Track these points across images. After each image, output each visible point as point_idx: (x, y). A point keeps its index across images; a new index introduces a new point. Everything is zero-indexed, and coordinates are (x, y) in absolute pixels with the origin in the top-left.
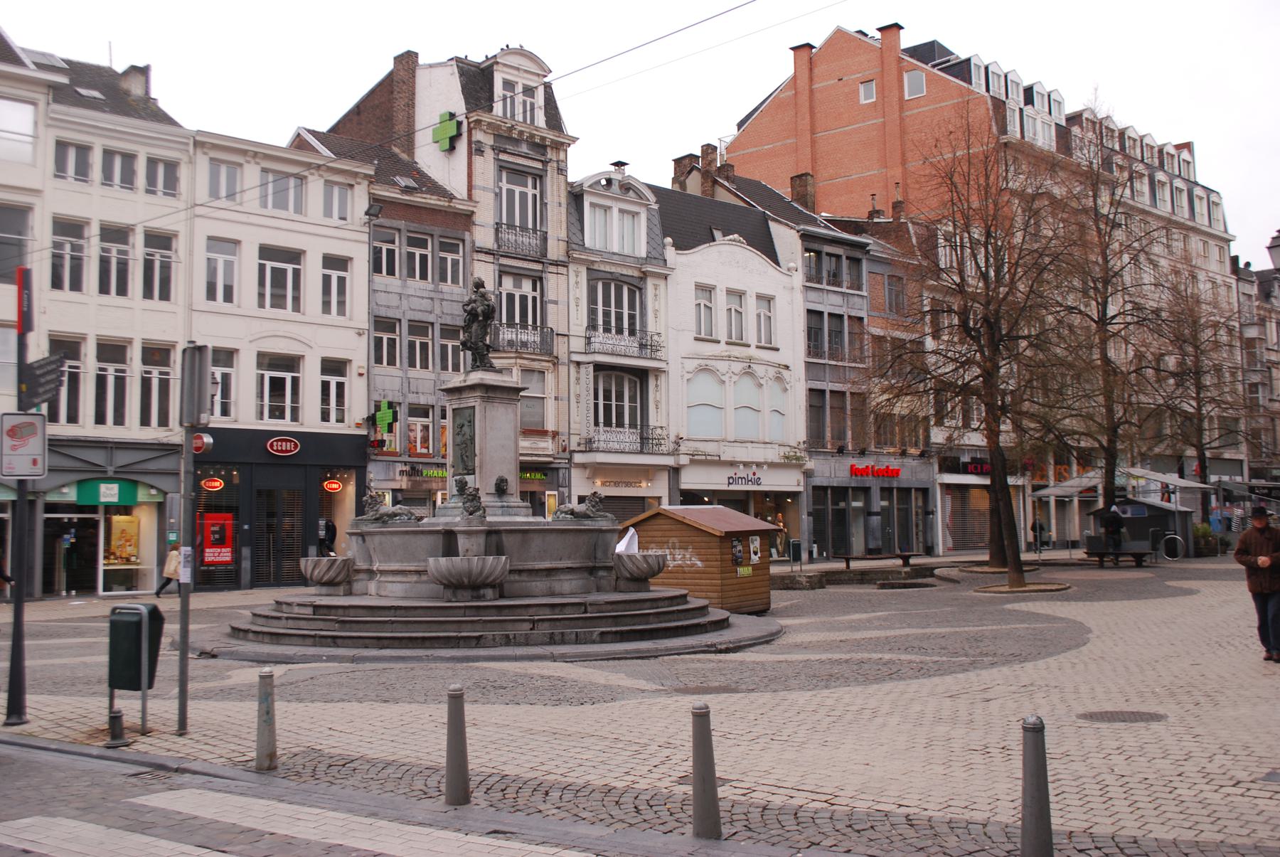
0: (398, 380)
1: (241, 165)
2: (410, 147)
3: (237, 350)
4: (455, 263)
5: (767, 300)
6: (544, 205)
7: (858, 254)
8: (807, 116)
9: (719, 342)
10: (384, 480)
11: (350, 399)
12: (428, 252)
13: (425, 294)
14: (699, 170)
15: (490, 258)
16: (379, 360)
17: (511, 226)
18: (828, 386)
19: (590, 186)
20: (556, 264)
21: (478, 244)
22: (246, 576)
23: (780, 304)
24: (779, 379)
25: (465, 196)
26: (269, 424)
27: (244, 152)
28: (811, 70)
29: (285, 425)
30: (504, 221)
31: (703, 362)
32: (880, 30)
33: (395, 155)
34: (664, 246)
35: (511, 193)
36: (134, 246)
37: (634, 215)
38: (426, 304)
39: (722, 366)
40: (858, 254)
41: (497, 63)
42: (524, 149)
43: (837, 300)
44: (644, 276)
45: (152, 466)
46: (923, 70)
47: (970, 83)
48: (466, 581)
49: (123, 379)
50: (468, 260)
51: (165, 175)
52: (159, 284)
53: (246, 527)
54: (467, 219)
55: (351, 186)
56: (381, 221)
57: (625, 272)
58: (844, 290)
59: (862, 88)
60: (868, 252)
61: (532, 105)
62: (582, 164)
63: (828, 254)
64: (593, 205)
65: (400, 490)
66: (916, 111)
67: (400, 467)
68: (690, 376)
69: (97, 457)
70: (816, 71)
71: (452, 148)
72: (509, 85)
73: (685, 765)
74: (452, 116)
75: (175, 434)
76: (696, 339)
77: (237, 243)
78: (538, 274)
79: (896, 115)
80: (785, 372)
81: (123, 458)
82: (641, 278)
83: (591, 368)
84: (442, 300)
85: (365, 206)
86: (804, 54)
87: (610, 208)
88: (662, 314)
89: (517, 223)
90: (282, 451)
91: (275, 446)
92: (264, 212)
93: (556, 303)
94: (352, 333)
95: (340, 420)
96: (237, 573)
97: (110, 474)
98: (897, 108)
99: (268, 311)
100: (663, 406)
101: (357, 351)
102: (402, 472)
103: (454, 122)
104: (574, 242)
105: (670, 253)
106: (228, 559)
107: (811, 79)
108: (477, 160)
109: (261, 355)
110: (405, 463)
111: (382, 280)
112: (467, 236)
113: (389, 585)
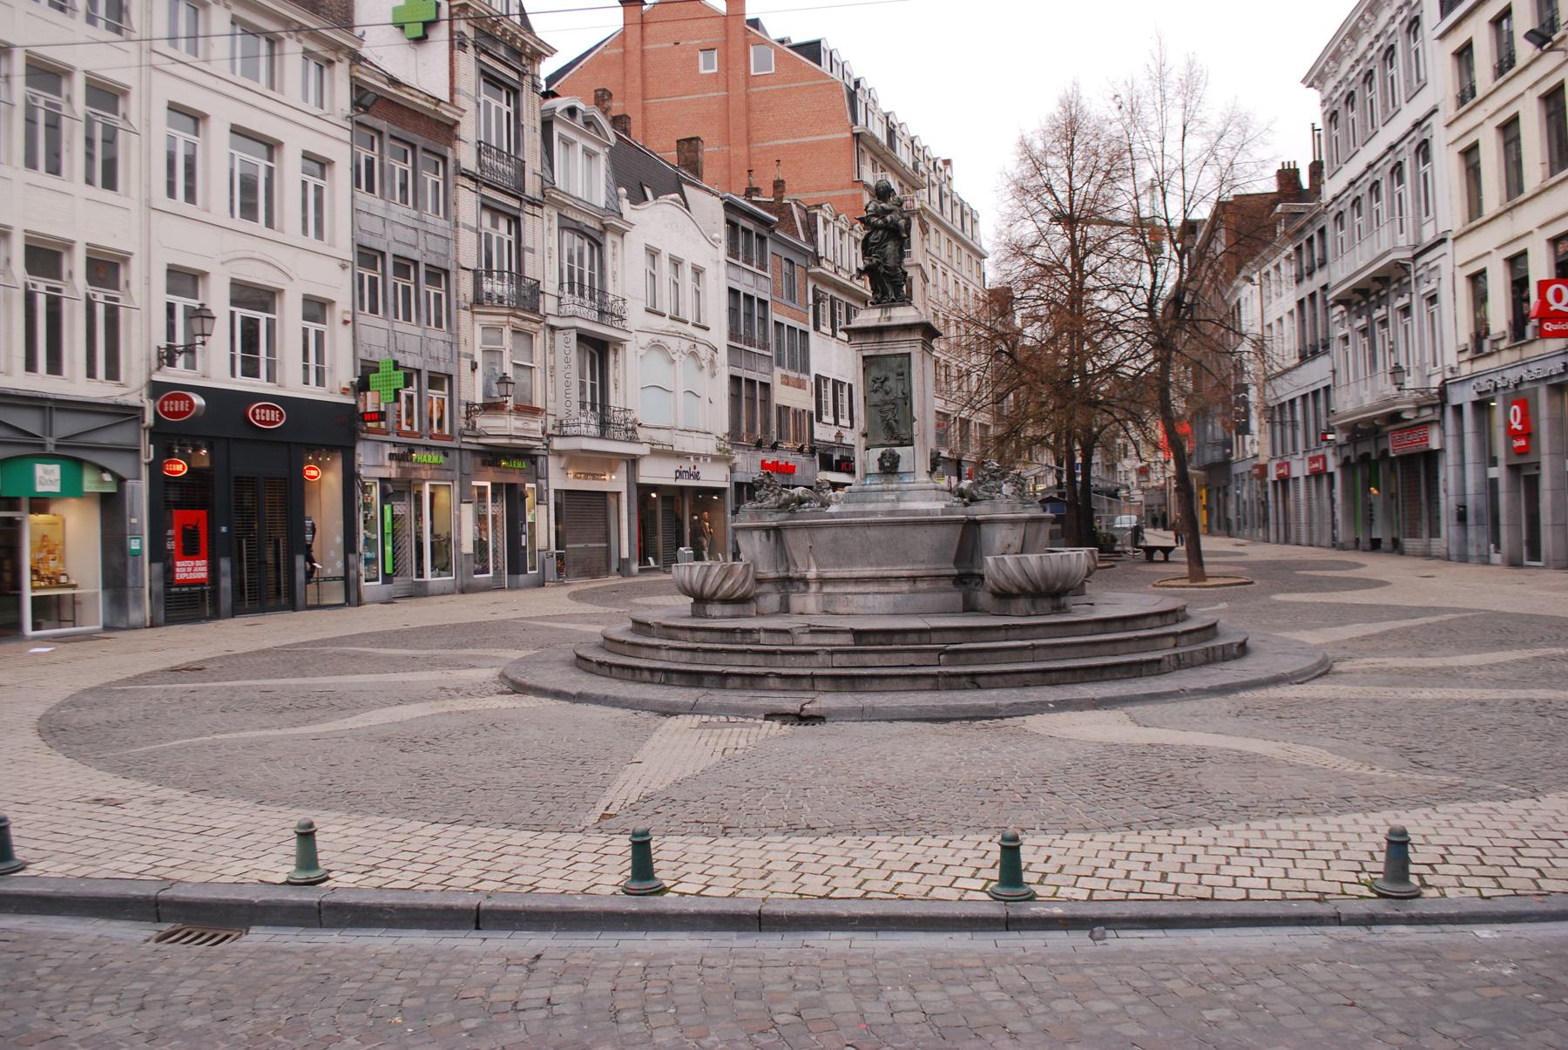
0: (384, 334)
3: (205, 274)
5: (698, 272)
6: (519, 126)
7: (764, 232)
8: (639, 81)
9: (663, 315)
10: (374, 462)
11: (128, 369)
13: (410, 223)
15: (472, 185)
20: (533, 203)
21: (463, 165)
22: (226, 600)
25: (445, 97)
26: (243, 384)
35: (487, 104)
36: (69, 99)
38: (409, 236)
39: (673, 343)
40: (764, 232)
42: (502, 52)
43: (748, 278)
44: (605, 228)
45: (104, 439)
48: (1043, 587)
50: (451, 185)
53: (224, 529)
55: (330, 63)
59: (701, 55)
63: (744, 229)
64: (561, 137)
65: (388, 480)
67: (389, 449)
69: (29, 421)
71: (421, 40)
75: (131, 389)
76: (648, 310)
78: (515, 213)
79: (742, 90)
81: (65, 425)
83: (573, 336)
84: (427, 232)
87: (573, 143)
90: (265, 422)
91: (261, 416)
93: (532, 251)
94: (335, 264)
95: (320, 382)
96: (215, 593)
97: (51, 449)
98: (743, 82)
100: (621, 385)
101: (338, 287)
102: (392, 456)
105: (625, 205)
106: (204, 575)
109: (236, 285)
110: (395, 444)
112: (449, 153)
113: (856, 598)
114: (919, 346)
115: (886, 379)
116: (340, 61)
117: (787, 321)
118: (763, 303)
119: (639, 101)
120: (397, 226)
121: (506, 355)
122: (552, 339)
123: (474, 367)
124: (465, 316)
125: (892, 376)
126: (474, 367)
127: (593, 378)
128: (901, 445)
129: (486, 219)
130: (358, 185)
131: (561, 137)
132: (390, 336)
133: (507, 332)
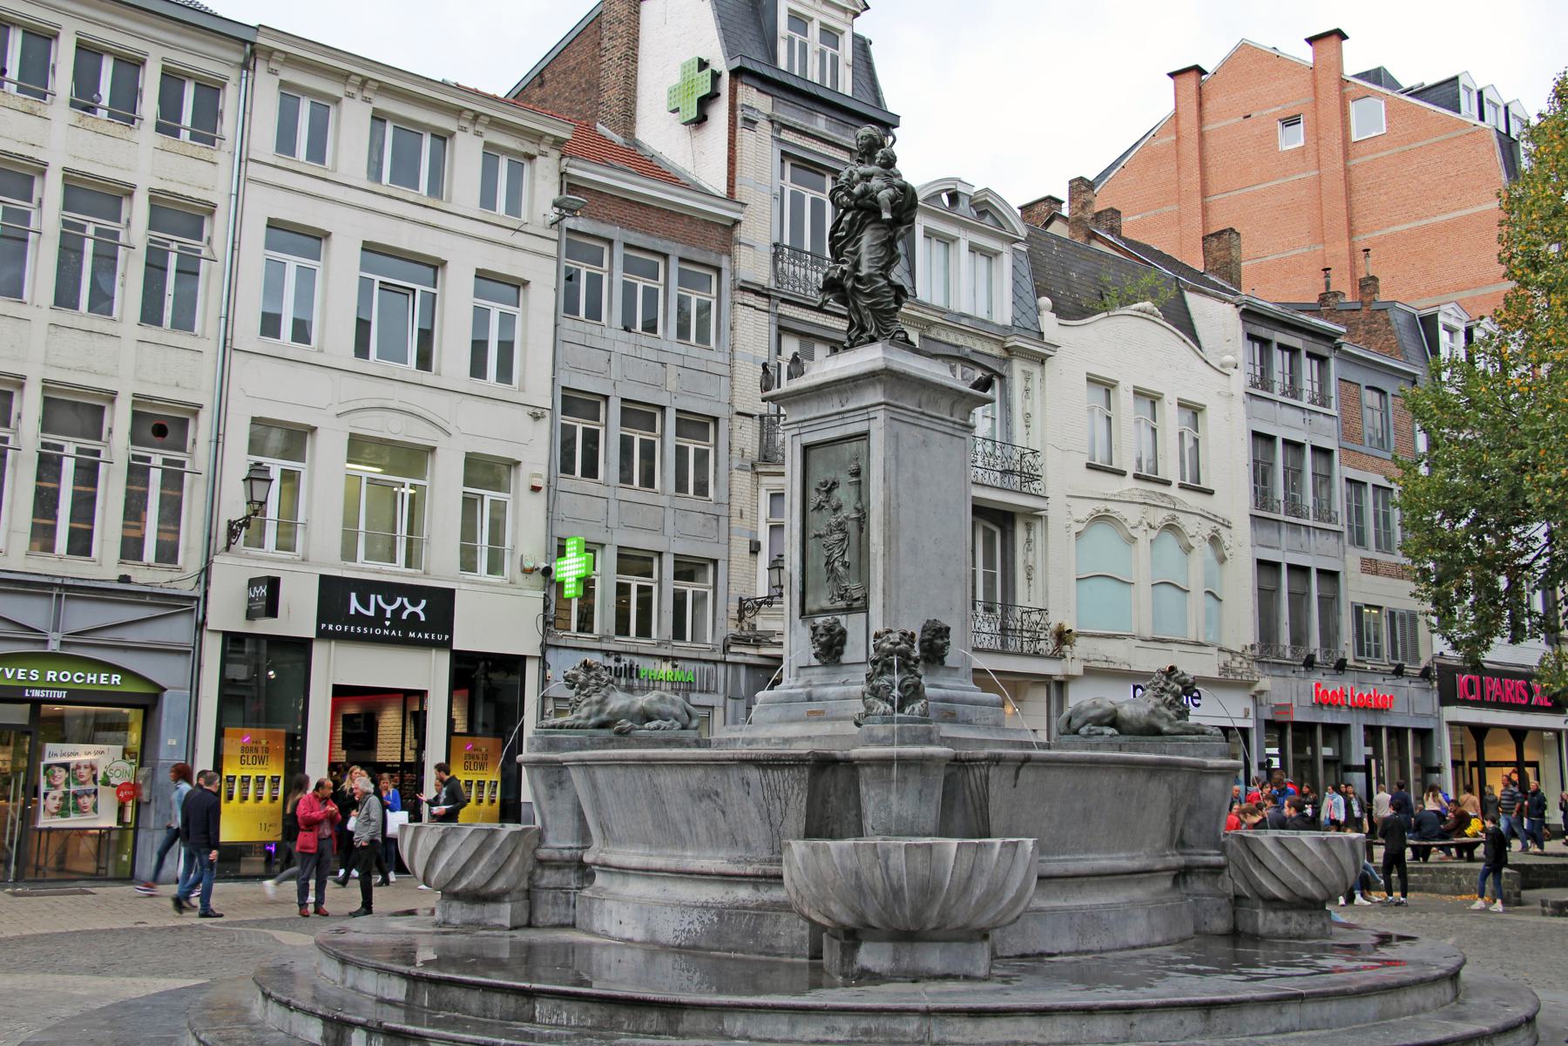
1: (337, 101)
2: (628, 118)
3: (313, 429)
4: (704, 309)
5: (1194, 410)
7: (1322, 349)
9: (1122, 473)
12: (659, 285)
14: (1065, 219)
15: (762, 303)
16: (567, 467)
17: (797, 251)
18: (1285, 558)
19: (925, 200)
23: (1212, 419)
24: (1214, 540)
25: (721, 188)
27: (345, 77)
28: (1200, 105)
29: (396, 572)
30: (787, 242)
31: (1101, 506)
32: (1310, 41)
33: (602, 137)
34: (1038, 311)
37: (991, 255)
40: (1322, 349)
46: (1379, 95)
47: (1459, 111)
49: (94, 467)
51: (194, 110)
52: (168, 299)
55: (531, 158)
57: (979, 347)
58: (1304, 404)
60: (1338, 347)
61: (835, 60)
63: (1282, 347)
66: (1371, 157)
68: (1080, 527)
70: (1208, 106)
71: (701, 120)
73: (227, 741)
74: (703, 65)
76: (1090, 467)
77: (321, 236)
79: (1339, 165)
80: (1224, 532)
82: (1005, 360)
85: (554, 194)
86: (1190, 81)
87: (954, 240)
88: (1036, 422)
89: (807, 248)
92: (376, 187)
94: (521, 414)
97: (53, 646)
98: (1339, 152)
99: (374, 364)
100: (1038, 575)
101: (535, 450)
107: (1201, 118)
108: (745, 137)
111: (579, 327)
112: (724, 263)
114: (881, 415)
115: (835, 484)
116: (544, 154)
118: (1323, 453)
119: (1198, 200)
120: (624, 364)
123: (755, 549)
124: (743, 480)
125: (844, 478)
126: (755, 549)
128: (849, 610)
132: (617, 510)
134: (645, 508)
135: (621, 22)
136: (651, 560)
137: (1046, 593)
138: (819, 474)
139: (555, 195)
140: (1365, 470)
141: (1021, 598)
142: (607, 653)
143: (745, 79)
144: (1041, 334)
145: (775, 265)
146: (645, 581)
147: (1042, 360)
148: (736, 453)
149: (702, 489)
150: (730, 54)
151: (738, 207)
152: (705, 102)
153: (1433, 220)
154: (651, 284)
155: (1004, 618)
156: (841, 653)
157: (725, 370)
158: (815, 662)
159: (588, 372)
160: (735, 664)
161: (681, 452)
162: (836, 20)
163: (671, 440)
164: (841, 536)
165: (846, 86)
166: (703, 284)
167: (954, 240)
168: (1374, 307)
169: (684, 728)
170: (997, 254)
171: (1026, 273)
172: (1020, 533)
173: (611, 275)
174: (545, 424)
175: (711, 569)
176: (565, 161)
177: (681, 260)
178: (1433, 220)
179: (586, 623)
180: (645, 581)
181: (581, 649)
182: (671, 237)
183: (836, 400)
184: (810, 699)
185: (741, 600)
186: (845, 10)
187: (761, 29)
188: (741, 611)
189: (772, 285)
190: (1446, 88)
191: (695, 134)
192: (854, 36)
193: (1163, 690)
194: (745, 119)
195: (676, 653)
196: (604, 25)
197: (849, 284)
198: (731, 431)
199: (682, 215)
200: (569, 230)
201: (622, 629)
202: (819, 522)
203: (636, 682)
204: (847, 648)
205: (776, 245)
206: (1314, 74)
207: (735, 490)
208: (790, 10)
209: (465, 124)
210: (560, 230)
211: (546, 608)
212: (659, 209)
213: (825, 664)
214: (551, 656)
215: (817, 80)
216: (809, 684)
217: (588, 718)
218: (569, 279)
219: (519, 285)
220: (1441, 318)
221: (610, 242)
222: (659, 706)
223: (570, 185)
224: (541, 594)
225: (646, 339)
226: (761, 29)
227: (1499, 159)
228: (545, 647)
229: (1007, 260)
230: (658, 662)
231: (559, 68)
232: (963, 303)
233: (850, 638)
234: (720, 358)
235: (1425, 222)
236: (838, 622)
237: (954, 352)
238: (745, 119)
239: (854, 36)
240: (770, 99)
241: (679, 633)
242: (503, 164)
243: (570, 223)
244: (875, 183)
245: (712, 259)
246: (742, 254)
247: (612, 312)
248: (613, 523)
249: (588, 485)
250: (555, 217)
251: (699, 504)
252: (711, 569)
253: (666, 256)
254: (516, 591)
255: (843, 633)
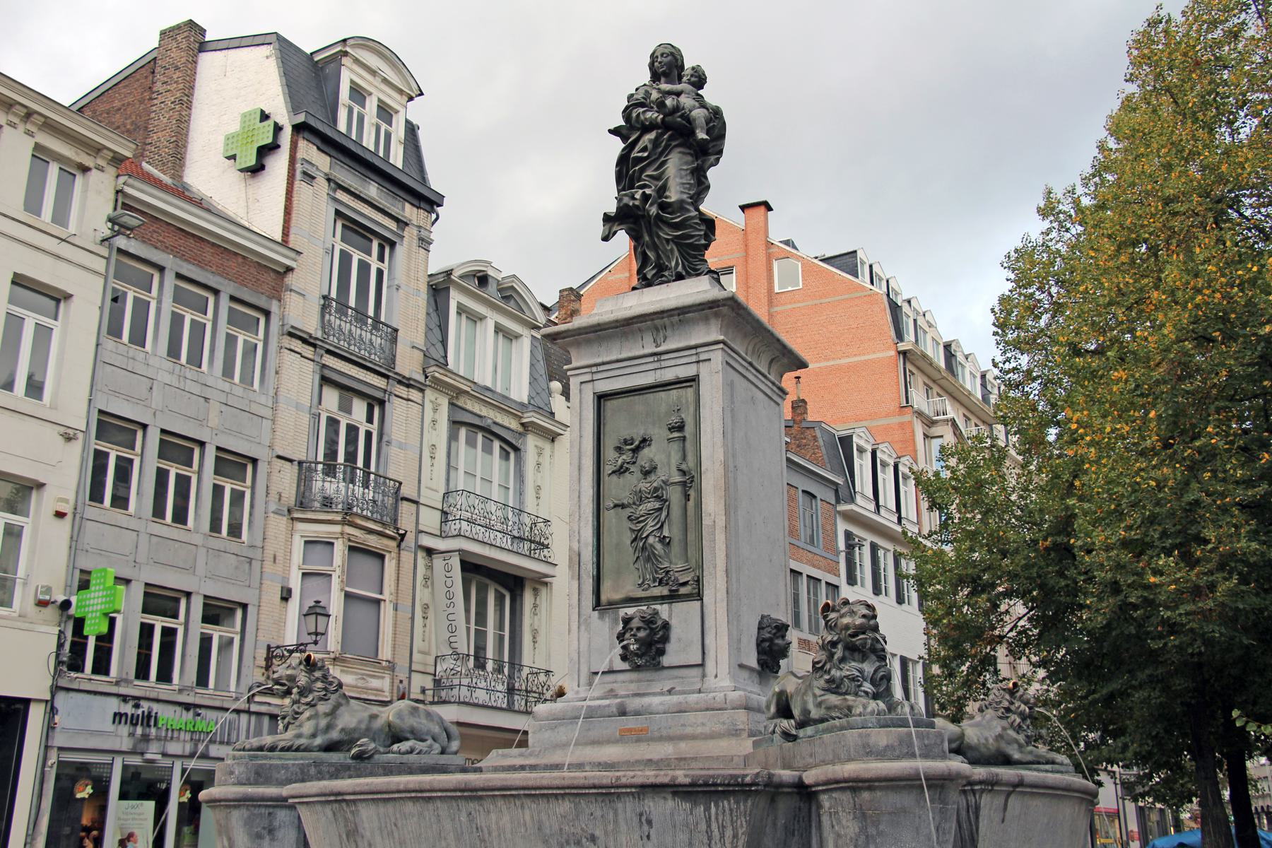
2: (178, 158)
15: (308, 351)
16: (96, 495)
17: (343, 306)
19: (461, 277)
20: (407, 383)
25: (278, 237)
37: (510, 337)
41: (346, 54)
54: (277, 276)
56: (133, 246)
57: (499, 420)
61: (388, 136)
62: (453, 242)
64: (461, 310)
66: (789, 307)
71: (257, 169)
72: (358, 94)
74: (264, 117)
78: (379, 395)
83: (455, 562)
87: (482, 318)
89: (352, 303)
94: (52, 434)
98: (765, 300)
101: (64, 473)
103: (269, 125)
104: (435, 355)
112: (274, 307)
114: (717, 356)
115: (645, 442)
116: (100, 169)
117: (807, 570)
120: (163, 394)
121: (335, 580)
122: (430, 567)
123: (286, 596)
124: (279, 524)
125: (659, 434)
126: (286, 596)
127: (501, 626)
128: (673, 597)
129: (331, 398)
130: (115, 331)
131: (461, 310)
132: (139, 548)
133: (340, 549)
134: (177, 545)
135: (177, 68)
136: (177, 600)
137: (549, 656)
138: (621, 425)
139: (109, 210)
140: (801, 561)
141: (527, 659)
142: (125, 698)
143: (306, 135)
144: (552, 414)
145: (323, 317)
146: (170, 622)
147: (553, 437)
148: (274, 496)
149: (235, 530)
150: (295, 108)
151: (293, 255)
152: (266, 151)
153: (838, 362)
154: (199, 318)
155: (511, 677)
156: (662, 652)
157: (267, 413)
158: (620, 665)
159: (128, 398)
160: (259, 714)
161: (218, 491)
162: (393, 100)
163: (209, 478)
164: (657, 505)
165: (397, 157)
166: (251, 326)
167: (482, 318)
168: (804, 425)
169: (443, 752)
170: (518, 337)
171: (540, 358)
172: (528, 598)
173: (159, 302)
174: (77, 446)
175: (239, 613)
176: (122, 179)
177: (233, 299)
178: (838, 362)
179: (102, 666)
180: (170, 622)
181: (96, 693)
182: (224, 274)
183: (648, 339)
184: (623, 712)
185: (269, 647)
186: (401, 92)
187: (321, 93)
188: (269, 659)
189: (319, 334)
190: (848, 259)
191: (250, 181)
192: (407, 121)
193: (1008, 710)
194: (305, 173)
195: (198, 701)
196: (158, 69)
197: (653, 210)
198: (269, 474)
199: (236, 254)
200: (120, 251)
201: (142, 672)
202: (618, 489)
203: (153, 730)
204: (671, 647)
205: (325, 297)
206: (746, 234)
207: (270, 534)
208: (352, 82)
209: (16, 120)
210: (110, 247)
211: (60, 645)
212: (213, 244)
213: (636, 668)
214: (61, 700)
215: (372, 148)
216: (611, 694)
217: (314, 736)
218: (115, 300)
219: (59, 298)
220: (855, 439)
221: (161, 269)
222: (411, 722)
223: (123, 201)
224: (56, 630)
225: (191, 373)
226: (321, 93)
227: (889, 318)
228: (55, 689)
229: (526, 343)
230: (178, 709)
231: (101, 107)
232: (484, 376)
233: (675, 634)
234: (263, 400)
235: (831, 363)
236: (656, 613)
237: (477, 421)
238: (305, 173)
239: (407, 121)
240: (328, 159)
241: (202, 680)
242: (54, 170)
243: (121, 242)
244: (686, 101)
245: (262, 302)
246: (292, 300)
247: (157, 340)
248: (142, 558)
249: (117, 515)
250: (108, 233)
251: (233, 546)
252: (239, 613)
253: (216, 292)
254: (26, 626)
255: (666, 626)
